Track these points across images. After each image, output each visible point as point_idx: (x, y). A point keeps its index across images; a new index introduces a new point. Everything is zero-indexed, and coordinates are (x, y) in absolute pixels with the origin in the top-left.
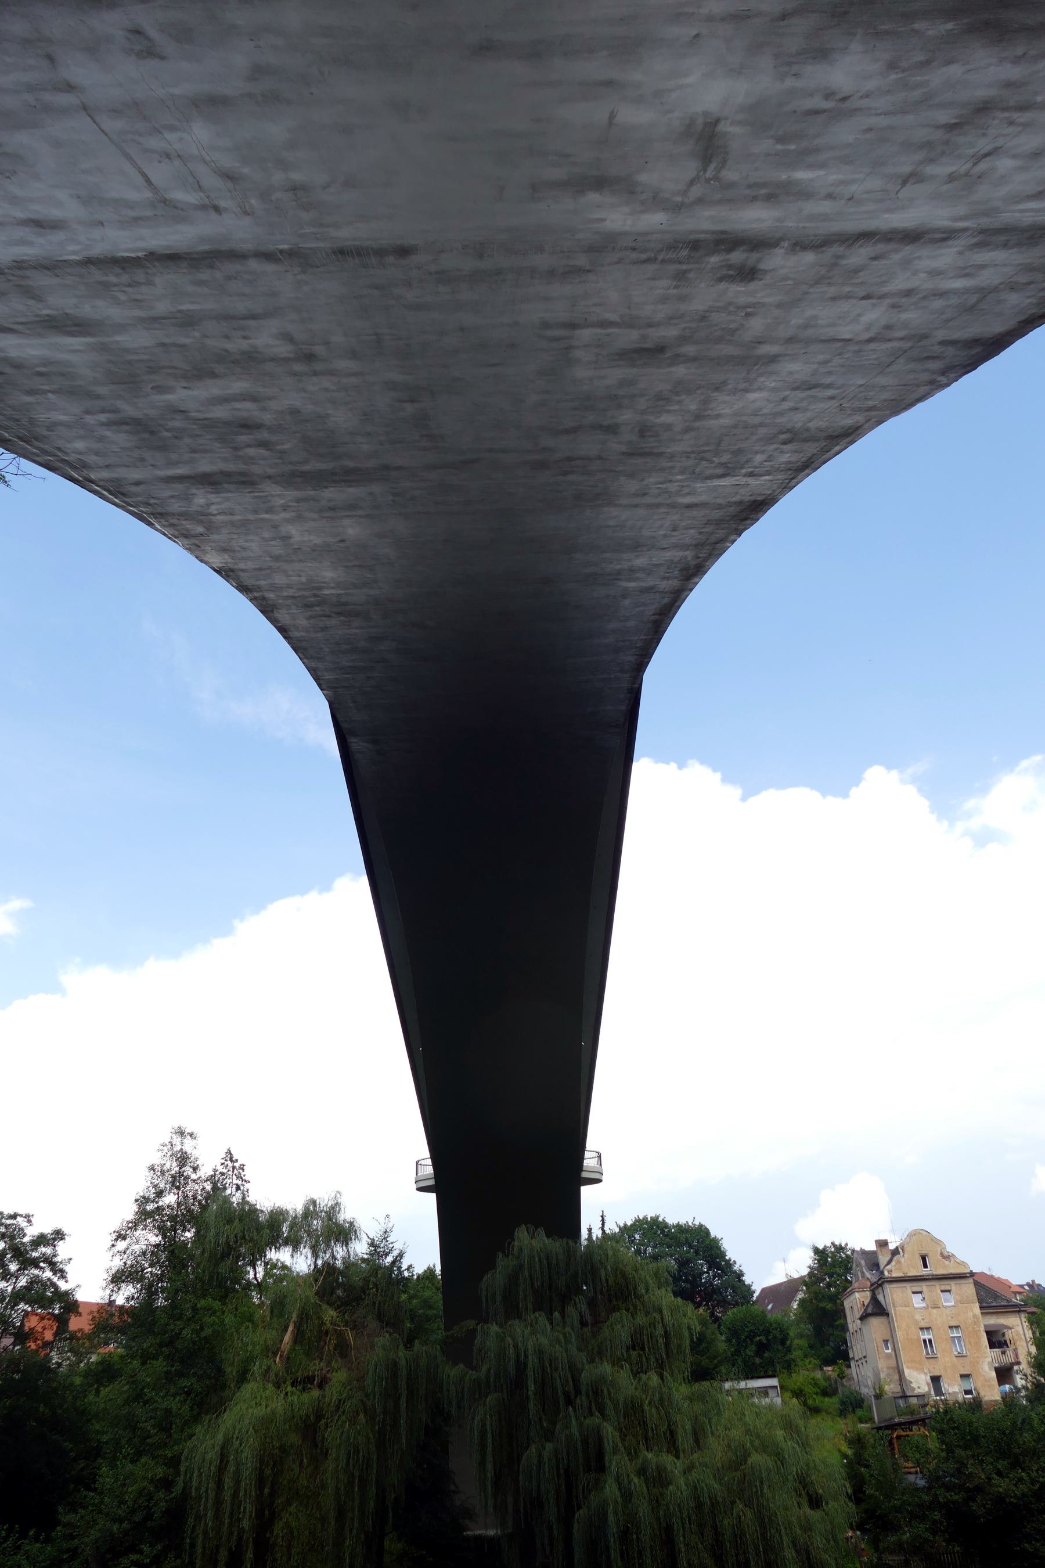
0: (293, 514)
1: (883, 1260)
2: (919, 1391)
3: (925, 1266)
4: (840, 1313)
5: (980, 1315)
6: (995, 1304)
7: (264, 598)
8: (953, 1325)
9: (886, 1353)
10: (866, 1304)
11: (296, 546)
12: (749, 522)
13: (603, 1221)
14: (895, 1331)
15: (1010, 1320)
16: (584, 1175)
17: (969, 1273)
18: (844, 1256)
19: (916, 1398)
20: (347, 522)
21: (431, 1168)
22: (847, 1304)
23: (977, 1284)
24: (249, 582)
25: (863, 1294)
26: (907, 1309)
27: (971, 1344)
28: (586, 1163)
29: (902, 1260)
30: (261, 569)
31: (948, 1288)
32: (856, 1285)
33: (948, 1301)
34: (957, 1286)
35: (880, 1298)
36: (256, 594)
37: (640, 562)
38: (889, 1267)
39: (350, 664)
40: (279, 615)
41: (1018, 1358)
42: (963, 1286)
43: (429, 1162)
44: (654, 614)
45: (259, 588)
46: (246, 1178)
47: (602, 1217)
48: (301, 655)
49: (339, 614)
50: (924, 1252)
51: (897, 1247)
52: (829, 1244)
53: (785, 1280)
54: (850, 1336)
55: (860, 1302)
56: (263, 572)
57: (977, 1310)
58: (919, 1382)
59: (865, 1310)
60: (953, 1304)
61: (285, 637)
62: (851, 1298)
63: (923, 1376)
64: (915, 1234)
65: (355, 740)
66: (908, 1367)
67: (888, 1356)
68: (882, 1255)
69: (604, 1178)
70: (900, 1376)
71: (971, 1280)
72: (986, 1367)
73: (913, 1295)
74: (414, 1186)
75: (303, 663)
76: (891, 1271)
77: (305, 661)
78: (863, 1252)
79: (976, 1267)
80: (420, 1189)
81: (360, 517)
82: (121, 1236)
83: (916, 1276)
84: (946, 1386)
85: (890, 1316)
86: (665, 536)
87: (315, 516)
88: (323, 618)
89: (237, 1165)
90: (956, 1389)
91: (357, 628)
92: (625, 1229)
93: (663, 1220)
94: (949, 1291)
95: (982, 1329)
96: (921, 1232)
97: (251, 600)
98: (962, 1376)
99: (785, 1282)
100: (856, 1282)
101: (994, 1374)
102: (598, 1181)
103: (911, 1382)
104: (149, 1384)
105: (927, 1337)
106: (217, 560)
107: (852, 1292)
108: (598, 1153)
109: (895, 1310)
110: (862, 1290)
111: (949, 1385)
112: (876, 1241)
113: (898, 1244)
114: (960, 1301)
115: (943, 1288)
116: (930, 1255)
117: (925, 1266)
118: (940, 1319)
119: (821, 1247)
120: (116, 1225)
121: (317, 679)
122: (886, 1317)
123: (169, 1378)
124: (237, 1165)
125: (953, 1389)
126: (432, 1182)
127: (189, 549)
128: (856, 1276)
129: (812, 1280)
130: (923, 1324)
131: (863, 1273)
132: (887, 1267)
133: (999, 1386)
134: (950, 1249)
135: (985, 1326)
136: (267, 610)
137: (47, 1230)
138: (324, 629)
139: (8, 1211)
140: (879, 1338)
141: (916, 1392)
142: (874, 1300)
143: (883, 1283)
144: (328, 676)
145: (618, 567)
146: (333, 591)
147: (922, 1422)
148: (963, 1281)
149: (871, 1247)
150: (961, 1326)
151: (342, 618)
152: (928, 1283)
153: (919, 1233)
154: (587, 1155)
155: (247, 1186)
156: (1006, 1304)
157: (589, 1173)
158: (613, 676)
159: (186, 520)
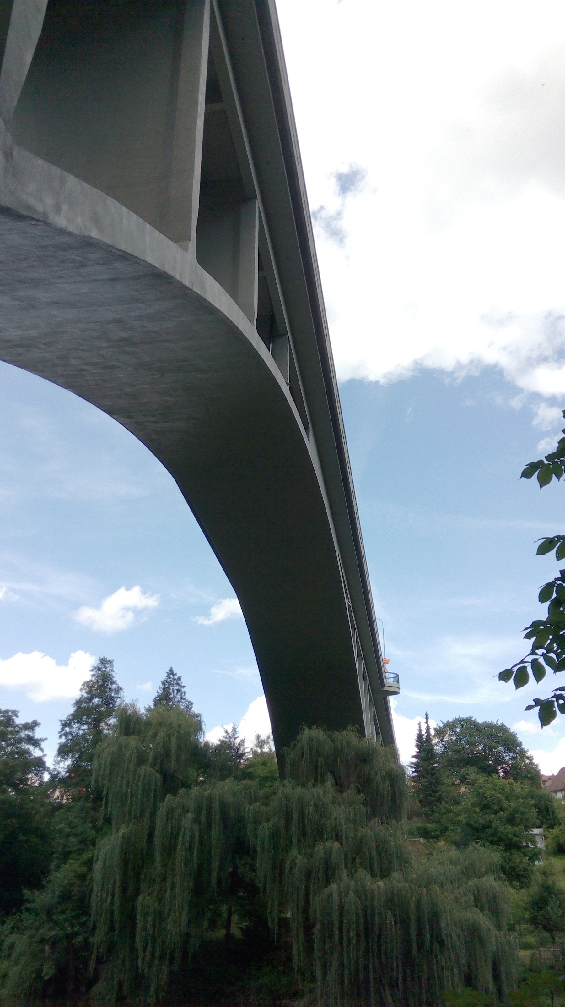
16: (386, 689)
46: (183, 685)
69: (401, 691)
82: (66, 724)
89: (176, 677)
93: (475, 719)
108: (397, 674)
119: (37, 728)
120: (64, 717)
124: (176, 677)
137: (30, 721)
139: (4, 709)
154: (388, 675)
155: (183, 690)
157: (390, 688)
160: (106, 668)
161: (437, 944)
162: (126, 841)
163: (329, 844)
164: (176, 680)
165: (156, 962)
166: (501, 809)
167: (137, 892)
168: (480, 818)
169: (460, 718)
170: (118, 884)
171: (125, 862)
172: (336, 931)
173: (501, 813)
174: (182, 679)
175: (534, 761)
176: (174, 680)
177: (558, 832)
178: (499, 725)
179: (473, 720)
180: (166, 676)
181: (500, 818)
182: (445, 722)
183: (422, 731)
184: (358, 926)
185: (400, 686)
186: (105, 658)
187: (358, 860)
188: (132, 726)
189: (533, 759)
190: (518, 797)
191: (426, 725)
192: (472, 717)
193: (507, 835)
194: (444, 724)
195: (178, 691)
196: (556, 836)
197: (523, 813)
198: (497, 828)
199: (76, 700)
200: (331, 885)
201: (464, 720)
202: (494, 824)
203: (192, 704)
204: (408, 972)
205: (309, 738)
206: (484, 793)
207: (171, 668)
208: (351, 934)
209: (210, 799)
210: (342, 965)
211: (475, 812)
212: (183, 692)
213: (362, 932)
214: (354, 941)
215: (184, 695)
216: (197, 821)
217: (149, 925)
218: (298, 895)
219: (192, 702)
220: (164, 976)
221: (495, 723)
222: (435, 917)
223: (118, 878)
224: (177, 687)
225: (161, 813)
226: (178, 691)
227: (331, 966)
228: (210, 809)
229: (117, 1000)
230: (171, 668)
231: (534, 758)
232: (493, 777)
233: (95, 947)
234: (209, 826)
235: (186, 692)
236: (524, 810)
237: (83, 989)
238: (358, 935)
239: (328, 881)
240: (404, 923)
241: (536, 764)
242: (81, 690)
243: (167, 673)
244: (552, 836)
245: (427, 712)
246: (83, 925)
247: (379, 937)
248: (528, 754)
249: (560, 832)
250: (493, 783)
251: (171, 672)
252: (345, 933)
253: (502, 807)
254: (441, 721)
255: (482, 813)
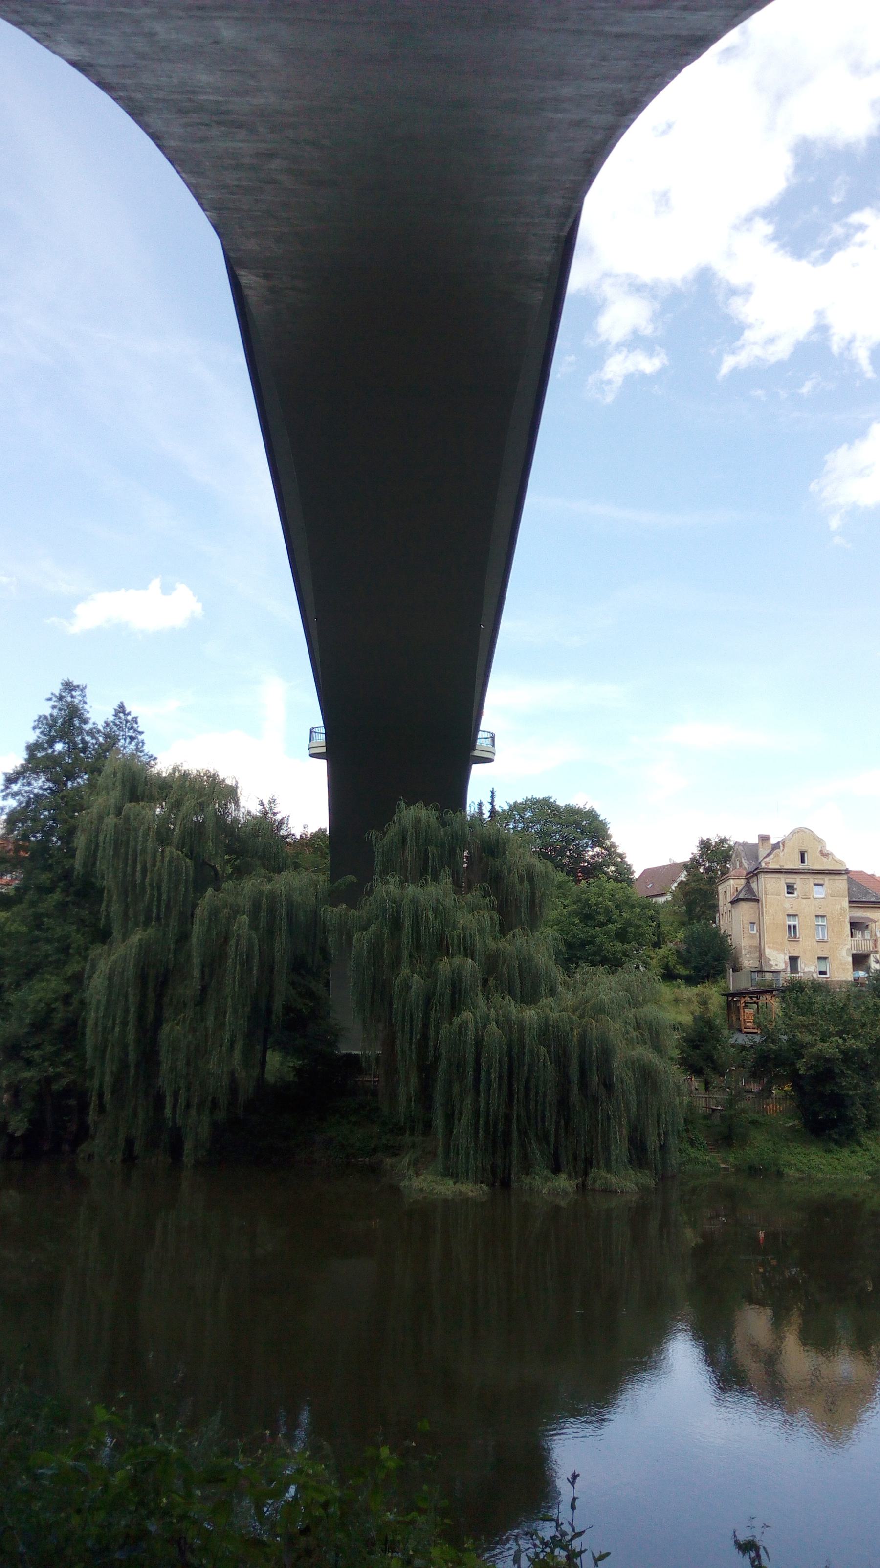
0: (156, 10)
1: (762, 852)
2: (776, 967)
3: (803, 861)
4: (714, 894)
5: (848, 908)
6: (864, 900)
7: (130, 99)
8: (820, 914)
9: (751, 934)
10: (739, 889)
11: (162, 44)
12: (690, 57)
13: (493, 797)
14: (763, 916)
15: (876, 914)
16: (476, 753)
17: (845, 871)
18: (726, 846)
19: (771, 974)
20: (219, 23)
21: (324, 736)
22: (721, 889)
23: (850, 881)
24: (114, 80)
25: (738, 881)
26: (778, 897)
27: (833, 932)
28: (479, 742)
29: (781, 854)
30: (124, 66)
31: (821, 882)
32: (732, 873)
33: (818, 893)
34: (831, 881)
35: (754, 885)
36: (121, 94)
37: (567, 91)
38: (767, 860)
39: (236, 183)
40: (150, 119)
41: (876, 947)
42: (836, 881)
43: (322, 730)
44: (584, 152)
45: (124, 88)
46: (140, 730)
47: (492, 792)
48: (179, 168)
49: (219, 123)
50: (803, 849)
51: (778, 843)
52: (612, 840)
53: (669, 863)
54: (719, 917)
55: (734, 888)
56: (128, 70)
57: (845, 903)
58: (778, 960)
59: (738, 895)
60: (823, 896)
61: (159, 146)
62: (727, 883)
63: (782, 956)
64: (798, 832)
65: (243, 273)
66: (769, 947)
67: (753, 936)
68: (763, 848)
69: (496, 758)
70: (761, 954)
71: (845, 877)
72: (844, 953)
73: (814, 887)
74: (308, 753)
75: (182, 177)
76: (769, 863)
77: (184, 175)
78: (745, 845)
79: (852, 866)
80: (312, 756)
81: (237, 19)
83: (791, 869)
84: (803, 966)
85: (760, 902)
86: (592, 65)
87: (181, 14)
88: (200, 127)
89: (129, 718)
90: (812, 969)
91: (242, 141)
92: (516, 808)
93: (555, 801)
94: (821, 885)
95: (847, 920)
96: (805, 830)
97: (115, 99)
98: (819, 958)
99: (667, 866)
100: (733, 870)
101: (850, 959)
102: (489, 760)
103: (770, 960)
104: (729, 1053)
105: (792, 923)
106: (72, 53)
107: (728, 879)
108: (492, 734)
109: (766, 898)
110: (738, 877)
111: (805, 965)
112: (759, 836)
113: (780, 840)
114: (831, 894)
115: (817, 882)
116: (809, 851)
117: (803, 861)
118: (807, 909)
121: (197, 197)
122: (756, 903)
123: (62, 906)
125: (808, 969)
126: (323, 750)
127: (37, 40)
128: (734, 864)
129: (691, 866)
130: (791, 912)
131: (741, 863)
132: (765, 860)
133: (854, 970)
134: (829, 848)
135: (850, 918)
136: (136, 112)
138: (203, 140)
140: (747, 919)
141: (773, 968)
142: (748, 886)
143: (758, 873)
144: (211, 195)
145: (541, 95)
146: (211, 98)
147: (769, 991)
148: (837, 877)
149: (755, 841)
150: (800, 915)
151: (223, 129)
152: (802, 876)
153: (804, 831)
154: (480, 735)
155: (140, 737)
156: (875, 900)
157: (483, 752)
158: (537, 221)
159: (31, 7)
160: (72, 697)
161: (604, 1089)
162: (145, 949)
163: (457, 960)
164: (129, 722)
165: (193, 1112)
166: (610, 921)
167: (158, 1022)
168: (580, 931)
169: (534, 799)
170: (132, 1009)
171: (142, 978)
172: (470, 1072)
173: (610, 925)
174: (139, 720)
175: (626, 859)
176: (127, 721)
177: (667, 952)
178: (587, 810)
179: (551, 802)
180: (114, 715)
181: (606, 933)
182: (512, 803)
183: (484, 814)
184: (501, 1067)
185: (495, 750)
186: (63, 682)
187: (491, 982)
188: (140, 789)
189: (625, 857)
190: (633, 906)
191: (489, 807)
192: (550, 798)
193: (614, 954)
194: (510, 806)
195: (132, 738)
196: (664, 957)
197: (639, 926)
198: (602, 944)
199: (28, 743)
200: (462, 1014)
201: (538, 801)
202: (598, 940)
203: (155, 759)
204: (562, 1122)
205: (416, 818)
206: (588, 900)
207: (122, 703)
208: (492, 1075)
209: (273, 897)
210: (476, 1113)
211: (573, 924)
212: (140, 740)
213: (505, 1073)
214: (495, 1085)
215: (142, 746)
216: (254, 924)
217: (181, 1064)
218: (412, 1026)
219: (155, 756)
220: (205, 1131)
221: (582, 807)
222: (606, 1053)
223: (133, 1000)
224: (131, 733)
225: (201, 912)
226: (132, 738)
227: (461, 1114)
228: (272, 911)
229: (124, 1161)
230: (122, 703)
231: (627, 855)
232: (600, 878)
233: (95, 1093)
234: (271, 932)
235: (145, 741)
236: (640, 923)
237: (66, 1147)
238: (500, 1077)
239: (455, 1008)
240: (561, 1061)
241: (629, 863)
242: (34, 728)
243: (115, 710)
244: (659, 957)
245: (493, 788)
246: (67, 1063)
247: (527, 1081)
248: (619, 851)
249: (669, 953)
250: (599, 886)
251: (121, 709)
252: (483, 1074)
253: (611, 918)
254: (506, 802)
255: (582, 925)
